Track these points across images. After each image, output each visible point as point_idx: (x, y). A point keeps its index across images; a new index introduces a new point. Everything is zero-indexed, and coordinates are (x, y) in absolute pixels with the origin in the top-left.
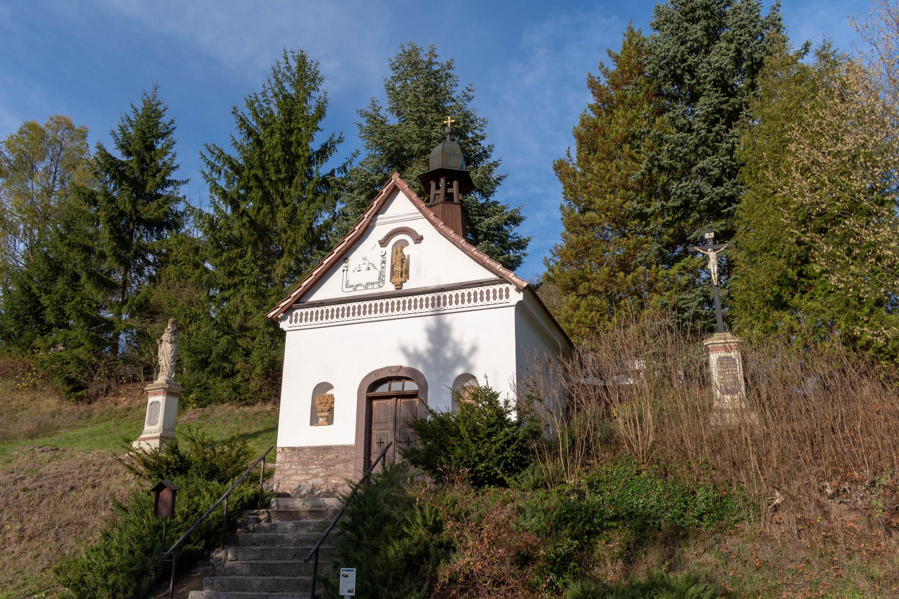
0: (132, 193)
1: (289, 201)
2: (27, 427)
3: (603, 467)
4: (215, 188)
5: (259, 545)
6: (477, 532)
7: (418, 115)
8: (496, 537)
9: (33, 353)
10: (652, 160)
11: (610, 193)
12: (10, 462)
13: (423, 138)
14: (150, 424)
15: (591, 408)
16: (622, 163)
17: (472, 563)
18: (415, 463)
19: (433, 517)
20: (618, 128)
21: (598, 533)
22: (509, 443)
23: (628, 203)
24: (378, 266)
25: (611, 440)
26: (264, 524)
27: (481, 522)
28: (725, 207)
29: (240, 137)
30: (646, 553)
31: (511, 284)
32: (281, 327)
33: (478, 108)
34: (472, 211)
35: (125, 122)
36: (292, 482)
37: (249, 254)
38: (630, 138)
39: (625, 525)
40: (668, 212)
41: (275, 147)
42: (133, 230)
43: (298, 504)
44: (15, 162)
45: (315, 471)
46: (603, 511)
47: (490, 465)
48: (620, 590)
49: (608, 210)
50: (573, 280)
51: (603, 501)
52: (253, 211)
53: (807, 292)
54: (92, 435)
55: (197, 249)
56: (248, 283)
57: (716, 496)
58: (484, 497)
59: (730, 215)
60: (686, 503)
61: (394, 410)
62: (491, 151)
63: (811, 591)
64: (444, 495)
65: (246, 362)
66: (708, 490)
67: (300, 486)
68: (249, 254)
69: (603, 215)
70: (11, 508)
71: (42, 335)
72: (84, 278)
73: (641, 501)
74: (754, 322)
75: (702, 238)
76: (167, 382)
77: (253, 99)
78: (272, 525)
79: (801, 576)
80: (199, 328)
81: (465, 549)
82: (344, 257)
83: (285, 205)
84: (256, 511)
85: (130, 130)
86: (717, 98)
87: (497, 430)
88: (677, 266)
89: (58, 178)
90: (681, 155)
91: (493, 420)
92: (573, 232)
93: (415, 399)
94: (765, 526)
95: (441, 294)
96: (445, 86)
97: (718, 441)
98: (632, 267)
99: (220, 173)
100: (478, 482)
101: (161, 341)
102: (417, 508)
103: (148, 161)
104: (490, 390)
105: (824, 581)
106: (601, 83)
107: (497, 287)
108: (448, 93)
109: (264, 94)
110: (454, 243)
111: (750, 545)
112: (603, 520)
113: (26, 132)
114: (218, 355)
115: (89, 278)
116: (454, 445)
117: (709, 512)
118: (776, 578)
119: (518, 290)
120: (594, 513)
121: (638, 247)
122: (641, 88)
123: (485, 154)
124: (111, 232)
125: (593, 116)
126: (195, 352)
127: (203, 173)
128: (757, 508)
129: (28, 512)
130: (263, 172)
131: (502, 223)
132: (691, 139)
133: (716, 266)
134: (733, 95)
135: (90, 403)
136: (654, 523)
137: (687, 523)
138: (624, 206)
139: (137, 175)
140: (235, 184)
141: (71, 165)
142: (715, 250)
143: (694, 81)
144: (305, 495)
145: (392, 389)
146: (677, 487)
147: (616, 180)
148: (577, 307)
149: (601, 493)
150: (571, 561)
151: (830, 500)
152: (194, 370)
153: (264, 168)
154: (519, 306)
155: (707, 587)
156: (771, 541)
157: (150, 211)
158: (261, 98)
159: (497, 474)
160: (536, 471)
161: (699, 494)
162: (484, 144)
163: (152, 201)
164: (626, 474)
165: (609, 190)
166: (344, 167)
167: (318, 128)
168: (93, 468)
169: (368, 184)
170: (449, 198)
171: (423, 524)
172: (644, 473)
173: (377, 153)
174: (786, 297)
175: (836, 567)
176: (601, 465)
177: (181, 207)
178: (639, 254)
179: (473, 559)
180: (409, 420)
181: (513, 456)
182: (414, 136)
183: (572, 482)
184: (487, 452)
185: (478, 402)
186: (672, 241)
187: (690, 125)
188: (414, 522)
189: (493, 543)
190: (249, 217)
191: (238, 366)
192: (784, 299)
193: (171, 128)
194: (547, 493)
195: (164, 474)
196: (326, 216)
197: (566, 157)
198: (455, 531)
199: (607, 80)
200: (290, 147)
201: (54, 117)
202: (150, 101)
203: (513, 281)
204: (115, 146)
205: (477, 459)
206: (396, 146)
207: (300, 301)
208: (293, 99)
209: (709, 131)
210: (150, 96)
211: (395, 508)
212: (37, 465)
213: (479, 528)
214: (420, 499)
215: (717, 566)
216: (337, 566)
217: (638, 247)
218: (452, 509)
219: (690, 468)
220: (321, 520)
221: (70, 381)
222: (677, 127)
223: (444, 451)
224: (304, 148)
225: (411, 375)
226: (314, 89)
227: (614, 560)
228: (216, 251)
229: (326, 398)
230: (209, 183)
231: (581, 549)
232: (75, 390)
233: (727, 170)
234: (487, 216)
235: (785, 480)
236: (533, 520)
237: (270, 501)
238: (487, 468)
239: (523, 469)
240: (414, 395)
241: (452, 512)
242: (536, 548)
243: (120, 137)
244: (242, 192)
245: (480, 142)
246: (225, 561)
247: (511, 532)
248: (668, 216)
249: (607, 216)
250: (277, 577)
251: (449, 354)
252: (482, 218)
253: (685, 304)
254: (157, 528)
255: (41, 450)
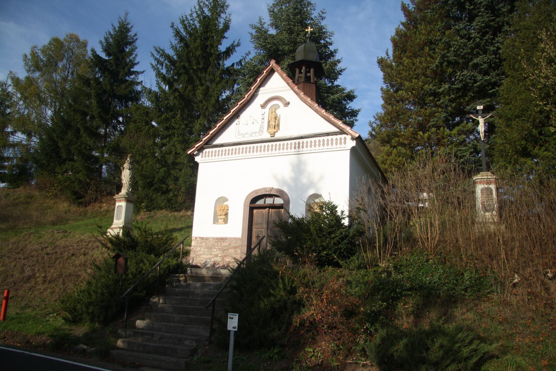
0: (111, 79)
1: (205, 83)
2: (51, 218)
3: (405, 256)
4: (159, 74)
5: (179, 296)
6: (319, 295)
7: (288, 27)
8: (332, 299)
9: (55, 176)
10: (443, 56)
11: (415, 78)
12: (41, 238)
13: (291, 42)
14: (117, 219)
15: (399, 219)
16: (423, 59)
17: (315, 314)
18: (280, 250)
19: (290, 284)
20: (421, 36)
21: (398, 298)
22: (343, 239)
23: (426, 86)
24: (260, 120)
25: (411, 240)
26: (182, 283)
27: (322, 289)
28: (490, 90)
29: (175, 41)
30: (429, 312)
31: (347, 134)
32: (196, 160)
33: (328, 24)
34: (323, 90)
35: (108, 35)
36: (201, 259)
37: (179, 115)
38: (428, 44)
39: (416, 293)
40: (453, 92)
41: (196, 49)
42: (111, 102)
43: (204, 272)
44: (46, 62)
45: (216, 253)
46: (403, 284)
47: (330, 252)
48: (412, 335)
49: (413, 89)
50: (388, 136)
51: (403, 278)
52: (182, 89)
53: (543, 145)
54: (86, 225)
55: (147, 113)
56: (177, 134)
57: (477, 276)
58: (324, 273)
59: (493, 95)
60: (457, 281)
61: (267, 216)
62: (336, 52)
63: (534, 337)
64: (298, 271)
65: (176, 184)
66: (471, 273)
67: (206, 262)
68: (179, 115)
69: (410, 93)
70: (40, 264)
71: (60, 165)
72: (82, 131)
73: (428, 279)
74: (507, 165)
75: (475, 109)
76: (127, 194)
77: (184, 19)
78: (187, 284)
79: (528, 328)
80: (147, 163)
81: (311, 305)
82: (238, 115)
83: (202, 85)
84: (178, 275)
85: (111, 40)
86: (488, 17)
87: (335, 230)
88: (457, 128)
89: (70, 72)
90: (462, 54)
91: (333, 223)
92: (390, 104)
93: (281, 210)
94: (507, 296)
95: (301, 141)
96: (307, 10)
97: (480, 241)
98: (427, 128)
99: (163, 65)
100: (321, 263)
101: (124, 168)
102: (280, 278)
103: (121, 59)
104: (332, 203)
105: (543, 331)
106: (410, 8)
107: (339, 137)
108: (309, 14)
109: (191, 15)
110: (310, 107)
111: (496, 308)
112: (403, 290)
113: (53, 44)
114: (159, 179)
115: (85, 131)
116: (306, 239)
117: (472, 287)
118: (512, 329)
119: (353, 139)
120: (397, 285)
121: (432, 115)
122: (436, 12)
123: (332, 54)
124: (98, 103)
125: (404, 29)
126: (144, 177)
127: (152, 65)
128: (503, 285)
129: (49, 267)
130: (189, 64)
131: (342, 99)
132: (470, 44)
133: (483, 128)
134: (498, 16)
135: (86, 206)
136: (436, 293)
137: (457, 293)
138: (424, 87)
139: (114, 68)
140: (172, 72)
141: (77, 63)
142: (483, 117)
143: (472, 7)
144: (209, 268)
145: (267, 203)
146: (452, 270)
147: (419, 71)
148: (389, 154)
149: (402, 273)
150: (380, 315)
151: (549, 281)
152: (145, 188)
153: (190, 62)
154: (353, 150)
155: (469, 334)
156: (510, 306)
157: (121, 90)
158: (189, 18)
159: (334, 259)
160: (360, 258)
161: (466, 275)
162: (332, 48)
163: (122, 84)
164: (419, 261)
165: (414, 76)
166: (240, 62)
167: (225, 37)
168: (85, 244)
169: (255, 71)
170: (308, 79)
171: (283, 288)
172: (431, 261)
173: (262, 52)
174: (530, 148)
175: (552, 323)
176: (403, 255)
177: (139, 88)
178: (432, 120)
179: (316, 312)
180: (277, 223)
181: (345, 247)
182: (286, 41)
183: (384, 265)
184: (328, 244)
185: (323, 211)
186: (454, 112)
187: (469, 36)
188: (277, 287)
189: (329, 303)
190: (179, 92)
191: (171, 187)
192: (529, 150)
193: (135, 38)
194: (367, 272)
195: (122, 249)
196: (228, 93)
197: (386, 55)
198: (305, 294)
199: (414, 6)
200: (207, 49)
201: (69, 34)
202: (123, 22)
203: (349, 133)
204: (101, 50)
205: (321, 249)
206: (274, 47)
207: (208, 144)
208: (209, 19)
209: (481, 39)
210: (123, 18)
211: (266, 278)
212: (55, 240)
213: (320, 292)
214: (282, 273)
215: (475, 321)
216: (227, 312)
217: (432, 115)
218: (303, 280)
219: (461, 259)
220: (218, 283)
221: (75, 193)
222: (460, 36)
223: (299, 243)
224: (215, 49)
225: (280, 194)
226: (223, 12)
227: (408, 316)
228: (158, 114)
229: (223, 207)
230: (155, 71)
231: (387, 308)
232: (78, 198)
233: (493, 65)
234: (333, 94)
235: (522, 267)
236: (357, 289)
237: (186, 269)
238: (327, 254)
239: (352, 256)
240: (280, 207)
241: (303, 281)
242: (358, 307)
243: (105, 44)
244: (176, 77)
245: (329, 46)
246: (158, 304)
247: (342, 295)
248: (453, 94)
249: (412, 93)
250: (189, 316)
251: (305, 180)
252: (329, 95)
253: (461, 153)
254: (117, 281)
255: (57, 231)
